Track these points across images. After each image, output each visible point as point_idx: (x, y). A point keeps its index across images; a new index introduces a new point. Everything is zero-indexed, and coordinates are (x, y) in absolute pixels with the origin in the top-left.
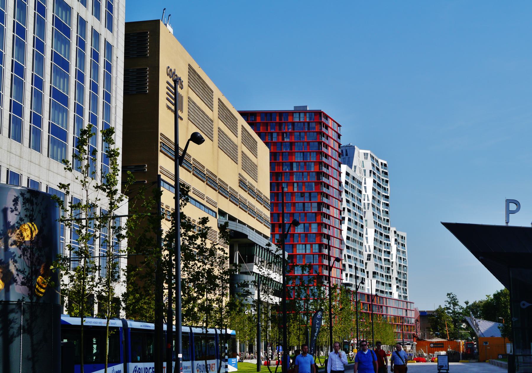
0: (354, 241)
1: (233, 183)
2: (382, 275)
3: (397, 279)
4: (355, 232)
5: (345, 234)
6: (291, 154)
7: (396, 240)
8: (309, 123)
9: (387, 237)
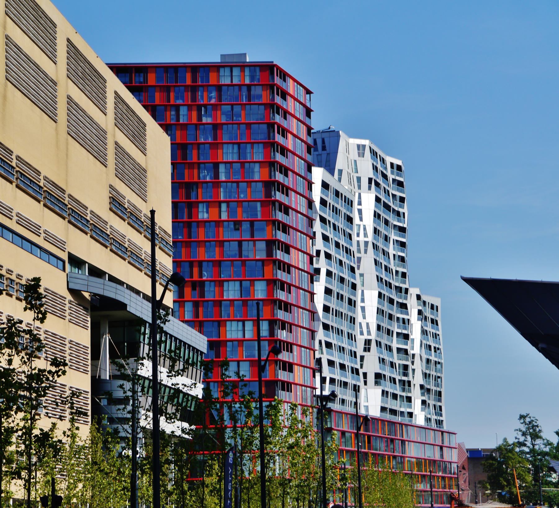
0: (339, 314)
1: (97, 204)
2: (393, 380)
3: (422, 387)
4: (340, 297)
5: (320, 301)
6: (216, 146)
7: (420, 312)
8: (249, 87)
9: (403, 306)
